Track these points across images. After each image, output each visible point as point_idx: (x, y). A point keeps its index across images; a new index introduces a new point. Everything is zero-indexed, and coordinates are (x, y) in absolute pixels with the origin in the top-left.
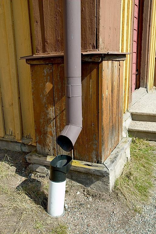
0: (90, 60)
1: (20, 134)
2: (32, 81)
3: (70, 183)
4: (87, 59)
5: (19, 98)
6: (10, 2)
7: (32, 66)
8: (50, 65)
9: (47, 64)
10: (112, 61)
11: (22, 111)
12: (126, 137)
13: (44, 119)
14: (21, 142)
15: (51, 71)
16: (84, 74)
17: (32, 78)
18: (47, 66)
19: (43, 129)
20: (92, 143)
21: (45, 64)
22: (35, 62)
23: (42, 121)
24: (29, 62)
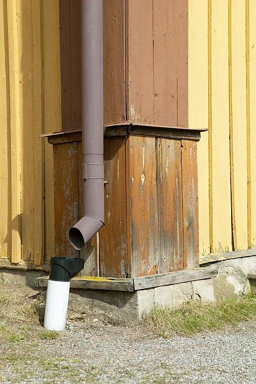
0: (115, 134)
1: (40, 256)
2: (54, 167)
3: (91, 312)
4: (113, 134)
5: (44, 198)
6: (42, 66)
7: (55, 145)
8: (75, 143)
9: (72, 142)
10: (156, 138)
11: (47, 220)
12: (201, 262)
13: (66, 219)
14: (41, 268)
15: (76, 151)
16: (108, 154)
17: (54, 162)
18: (72, 145)
19: (64, 236)
20: (120, 248)
21: (68, 143)
22: (58, 141)
23: (63, 223)
24: (51, 141)
